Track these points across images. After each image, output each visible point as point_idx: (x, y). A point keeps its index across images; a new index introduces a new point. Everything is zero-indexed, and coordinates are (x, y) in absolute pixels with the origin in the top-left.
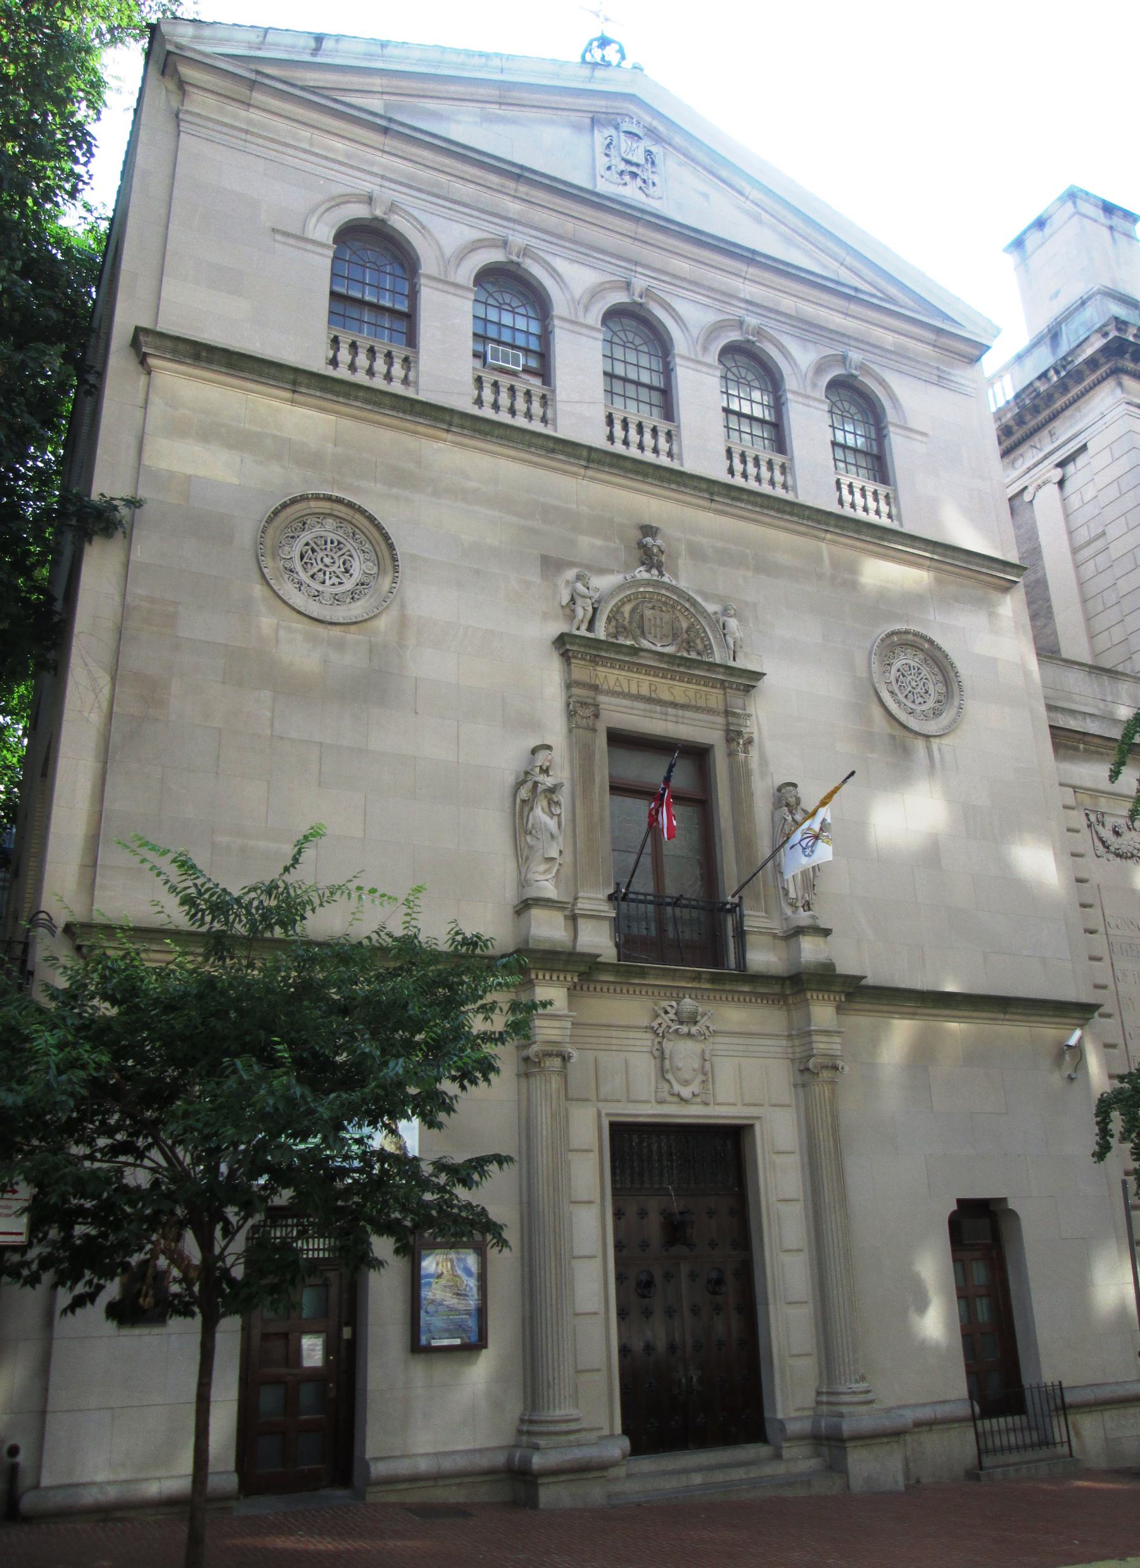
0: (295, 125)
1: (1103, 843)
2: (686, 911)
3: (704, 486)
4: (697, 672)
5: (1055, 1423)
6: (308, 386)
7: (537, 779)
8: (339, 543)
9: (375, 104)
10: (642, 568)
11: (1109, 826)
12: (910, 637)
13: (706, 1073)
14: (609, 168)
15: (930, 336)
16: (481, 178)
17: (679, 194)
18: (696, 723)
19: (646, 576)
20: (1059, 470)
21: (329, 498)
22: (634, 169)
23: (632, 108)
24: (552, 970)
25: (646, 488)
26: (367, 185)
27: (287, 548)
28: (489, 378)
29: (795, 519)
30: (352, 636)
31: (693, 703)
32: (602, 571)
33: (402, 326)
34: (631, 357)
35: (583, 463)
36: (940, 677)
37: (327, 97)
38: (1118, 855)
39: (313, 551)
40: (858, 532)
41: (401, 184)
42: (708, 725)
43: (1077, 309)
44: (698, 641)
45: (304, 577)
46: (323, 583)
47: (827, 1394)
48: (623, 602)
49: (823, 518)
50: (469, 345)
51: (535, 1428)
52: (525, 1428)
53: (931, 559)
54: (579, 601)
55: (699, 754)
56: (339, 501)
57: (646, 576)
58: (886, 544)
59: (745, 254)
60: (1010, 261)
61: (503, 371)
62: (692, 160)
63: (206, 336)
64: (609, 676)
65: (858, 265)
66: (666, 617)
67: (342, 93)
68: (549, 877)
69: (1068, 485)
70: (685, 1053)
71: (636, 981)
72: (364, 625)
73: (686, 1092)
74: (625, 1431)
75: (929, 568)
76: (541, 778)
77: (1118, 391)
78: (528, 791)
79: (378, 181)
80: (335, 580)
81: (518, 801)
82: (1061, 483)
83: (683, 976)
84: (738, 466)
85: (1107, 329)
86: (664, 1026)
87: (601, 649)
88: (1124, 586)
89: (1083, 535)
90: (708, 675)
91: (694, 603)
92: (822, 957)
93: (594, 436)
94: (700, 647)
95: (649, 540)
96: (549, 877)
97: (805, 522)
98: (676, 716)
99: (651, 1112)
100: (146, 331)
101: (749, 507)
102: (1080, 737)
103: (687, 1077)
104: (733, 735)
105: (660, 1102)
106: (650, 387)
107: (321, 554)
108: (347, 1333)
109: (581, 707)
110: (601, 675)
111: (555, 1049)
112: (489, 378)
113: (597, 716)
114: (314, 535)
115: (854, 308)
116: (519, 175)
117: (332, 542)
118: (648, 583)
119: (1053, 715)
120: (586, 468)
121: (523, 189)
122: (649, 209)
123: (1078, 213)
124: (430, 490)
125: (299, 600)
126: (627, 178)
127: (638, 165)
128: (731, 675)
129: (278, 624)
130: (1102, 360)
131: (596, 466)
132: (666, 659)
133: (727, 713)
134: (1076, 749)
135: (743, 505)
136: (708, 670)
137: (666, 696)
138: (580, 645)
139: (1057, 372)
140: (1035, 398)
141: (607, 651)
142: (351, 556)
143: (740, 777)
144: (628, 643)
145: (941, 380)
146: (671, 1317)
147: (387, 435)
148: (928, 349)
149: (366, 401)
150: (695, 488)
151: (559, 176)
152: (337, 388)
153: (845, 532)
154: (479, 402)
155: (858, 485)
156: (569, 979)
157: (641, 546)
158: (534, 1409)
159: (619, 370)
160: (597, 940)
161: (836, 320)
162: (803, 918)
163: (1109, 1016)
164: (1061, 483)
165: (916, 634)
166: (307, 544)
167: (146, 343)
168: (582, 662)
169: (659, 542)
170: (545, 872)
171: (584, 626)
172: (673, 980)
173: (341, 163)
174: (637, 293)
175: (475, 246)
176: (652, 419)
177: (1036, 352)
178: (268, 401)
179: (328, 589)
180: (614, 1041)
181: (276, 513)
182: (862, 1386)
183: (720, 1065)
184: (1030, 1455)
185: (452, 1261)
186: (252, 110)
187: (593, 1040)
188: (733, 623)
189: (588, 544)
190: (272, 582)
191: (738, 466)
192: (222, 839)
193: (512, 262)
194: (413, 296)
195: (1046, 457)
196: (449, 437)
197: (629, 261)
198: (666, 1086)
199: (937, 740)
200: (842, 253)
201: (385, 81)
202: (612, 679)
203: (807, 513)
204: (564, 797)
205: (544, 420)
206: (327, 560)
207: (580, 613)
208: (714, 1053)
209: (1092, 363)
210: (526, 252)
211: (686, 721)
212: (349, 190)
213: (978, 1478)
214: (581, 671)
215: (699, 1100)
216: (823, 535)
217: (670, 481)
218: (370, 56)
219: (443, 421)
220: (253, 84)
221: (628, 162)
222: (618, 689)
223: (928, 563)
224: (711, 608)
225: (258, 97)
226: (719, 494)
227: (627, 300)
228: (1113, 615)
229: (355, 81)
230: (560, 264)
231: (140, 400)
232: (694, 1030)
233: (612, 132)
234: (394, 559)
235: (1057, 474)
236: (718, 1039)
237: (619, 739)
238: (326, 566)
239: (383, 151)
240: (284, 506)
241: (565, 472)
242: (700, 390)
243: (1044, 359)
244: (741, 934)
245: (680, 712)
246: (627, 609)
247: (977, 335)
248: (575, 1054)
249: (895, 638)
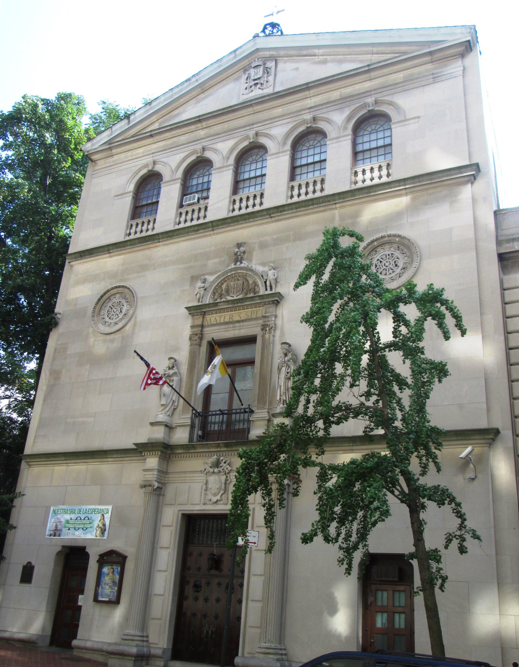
2: (238, 415)
3: (265, 213)
4: (246, 303)
6: (113, 249)
8: (392, 254)
9: (156, 126)
12: (386, 239)
16: (188, 130)
18: (249, 327)
24: (150, 451)
25: (240, 226)
29: (316, 206)
30: (117, 336)
35: (211, 229)
39: (381, 262)
40: (354, 196)
42: (255, 326)
46: (386, 274)
49: (331, 198)
53: (406, 189)
58: (372, 194)
59: (303, 87)
62: (291, 56)
65: (380, 49)
71: (192, 451)
72: (122, 330)
75: (406, 194)
79: (152, 156)
80: (391, 271)
83: (211, 446)
87: (203, 309)
90: (251, 303)
97: (322, 205)
98: (240, 326)
101: (290, 212)
105: (204, 504)
107: (384, 262)
111: (148, 483)
117: (389, 255)
120: (213, 230)
121: (204, 124)
122: (253, 98)
128: (263, 299)
131: (162, 240)
132: (230, 303)
135: (287, 212)
136: (251, 301)
138: (194, 310)
141: (205, 308)
142: (398, 258)
146: (206, 602)
148: (429, 66)
149: (131, 245)
150: (261, 216)
151: (225, 107)
152: (121, 245)
153: (346, 200)
165: (389, 236)
166: (378, 260)
168: (269, 305)
172: (208, 448)
178: (102, 260)
180: (188, 478)
185: (113, 569)
186: (114, 156)
187: (180, 479)
192: (69, 420)
196: (160, 244)
200: (370, 49)
201: (157, 116)
202: (213, 319)
203: (321, 200)
212: (141, 166)
216: (334, 206)
217: (249, 219)
219: (156, 239)
220: (110, 149)
223: (404, 192)
225: (114, 151)
226: (273, 213)
229: (146, 123)
238: (387, 267)
239: (154, 143)
241: (206, 236)
245: (242, 324)
247: (459, 39)
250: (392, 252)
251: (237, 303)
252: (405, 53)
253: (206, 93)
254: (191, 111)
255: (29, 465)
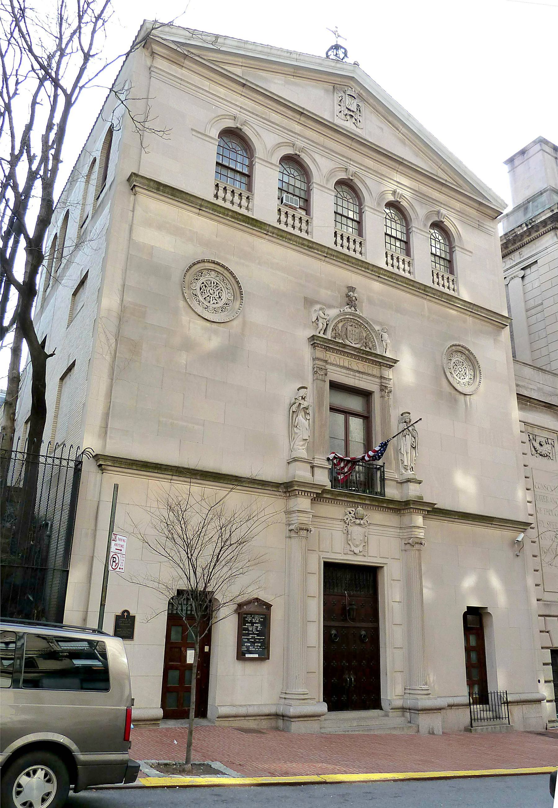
0: (202, 77)
1: (535, 449)
5: (503, 707)
7: (300, 402)
8: (217, 284)
9: (238, 71)
10: (347, 307)
11: (538, 441)
13: (366, 543)
14: (340, 112)
15: (476, 205)
17: (371, 128)
19: (349, 310)
20: (522, 271)
21: (213, 262)
22: (351, 113)
23: (352, 83)
26: (234, 111)
27: (194, 284)
28: (284, 209)
30: (221, 328)
31: (366, 372)
32: (330, 307)
33: (244, 180)
34: (233, 155)
36: (471, 367)
37: (217, 65)
38: (541, 455)
39: (206, 286)
41: (249, 111)
43: (538, 196)
44: (370, 343)
45: (201, 299)
47: (408, 690)
48: (339, 322)
50: (277, 193)
51: (287, 696)
52: (283, 696)
54: (321, 320)
55: (366, 395)
56: (218, 264)
57: (349, 310)
60: (506, 168)
61: (291, 207)
63: (161, 179)
64: (332, 357)
66: (357, 331)
67: (224, 64)
68: (304, 447)
69: (527, 279)
70: (357, 532)
73: (357, 551)
74: (324, 701)
76: (302, 402)
77: (555, 238)
78: (296, 409)
80: (463, 377)
81: (291, 412)
82: (523, 277)
84: (339, 241)
85: (553, 208)
86: (349, 519)
88: (549, 330)
89: (532, 303)
91: (370, 325)
92: (418, 494)
93: (271, 219)
94: (371, 346)
95: (351, 293)
96: (304, 447)
99: (342, 558)
100: (134, 174)
102: (528, 399)
103: (358, 543)
104: (383, 388)
106: (353, 220)
107: (209, 288)
108: (206, 649)
109: (319, 371)
110: (328, 355)
111: (305, 527)
112: (284, 209)
113: (326, 375)
114: (206, 279)
115: (444, 189)
116: (301, 113)
118: (350, 314)
119: (518, 388)
123: (542, 150)
124: (257, 261)
125: (199, 310)
126: (348, 117)
127: (353, 112)
129: (190, 320)
130: (549, 222)
133: (381, 377)
134: (526, 405)
137: (355, 368)
139: (527, 225)
140: (515, 236)
143: (385, 409)
144: (340, 341)
145: (480, 227)
147: (239, 234)
154: (216, 196)
155: (401, 258)
156: (312, 495)
157: (348, 296)
158: (287, 688)
159: (340, 211)
160: (323, 478)
161: (436, 195)
162: (409, 474)
163: (533, 528)
164: (523, 277)
166: (203, 283)
167: (136, 180)
169: (356, 295)
170: (302, 445)
171: (322, 332)
173: (222, 99)
174: (351, 173)
175: (279, 145)
176: (354, 236)
177: (516, 214)
179: (211, 306)
181: (190, 267)
182: (425, 687)
183: (369, 539)
184: (492, 722)
187: (329, 525)
188: (385, 336)
189: (325, 294)
190: (188, 300)
191: (339, 241)
193: (349, 179)
194: (251, 166)
195: (516, 265)
197: (347, 158)
198: (348, 546)
199: (469, 396)
201: (244, 60)
204: (310, 411)
205: (247, 208)
206: (212, 292)
207: (321, 325)
208: (370, 533)
209: (544, 223)
210: (354, 174)
211: (363, 380)
213: (470, 731)
214: (320, 353)
215: (361, 554)
216: (425, 297)
218: (238, 48)
220: (185, 56)
221: (349, 109)
222: (334, 362)
224: (377, 328)
225: (187, 63)
227: (394, 200)
228: (543, 343)
230: (317, 157)
231: (131, 208)
232: (362, 522)
233: (343, 94)
234: (241, 294)
235: (522, 273)
236: (371, 527)
237: (335, 386)
240: (194, 264)
242: (324, 202)
243: (521, 218)
244: (383, 480)
246: (340, 325)
248: (313, 529)
249: (454, 348)
250: (218, 282)
251: (363, 354)
252: (460, 187)
253: (297, 80)
254: (278, 86)
255: (102, 470)
